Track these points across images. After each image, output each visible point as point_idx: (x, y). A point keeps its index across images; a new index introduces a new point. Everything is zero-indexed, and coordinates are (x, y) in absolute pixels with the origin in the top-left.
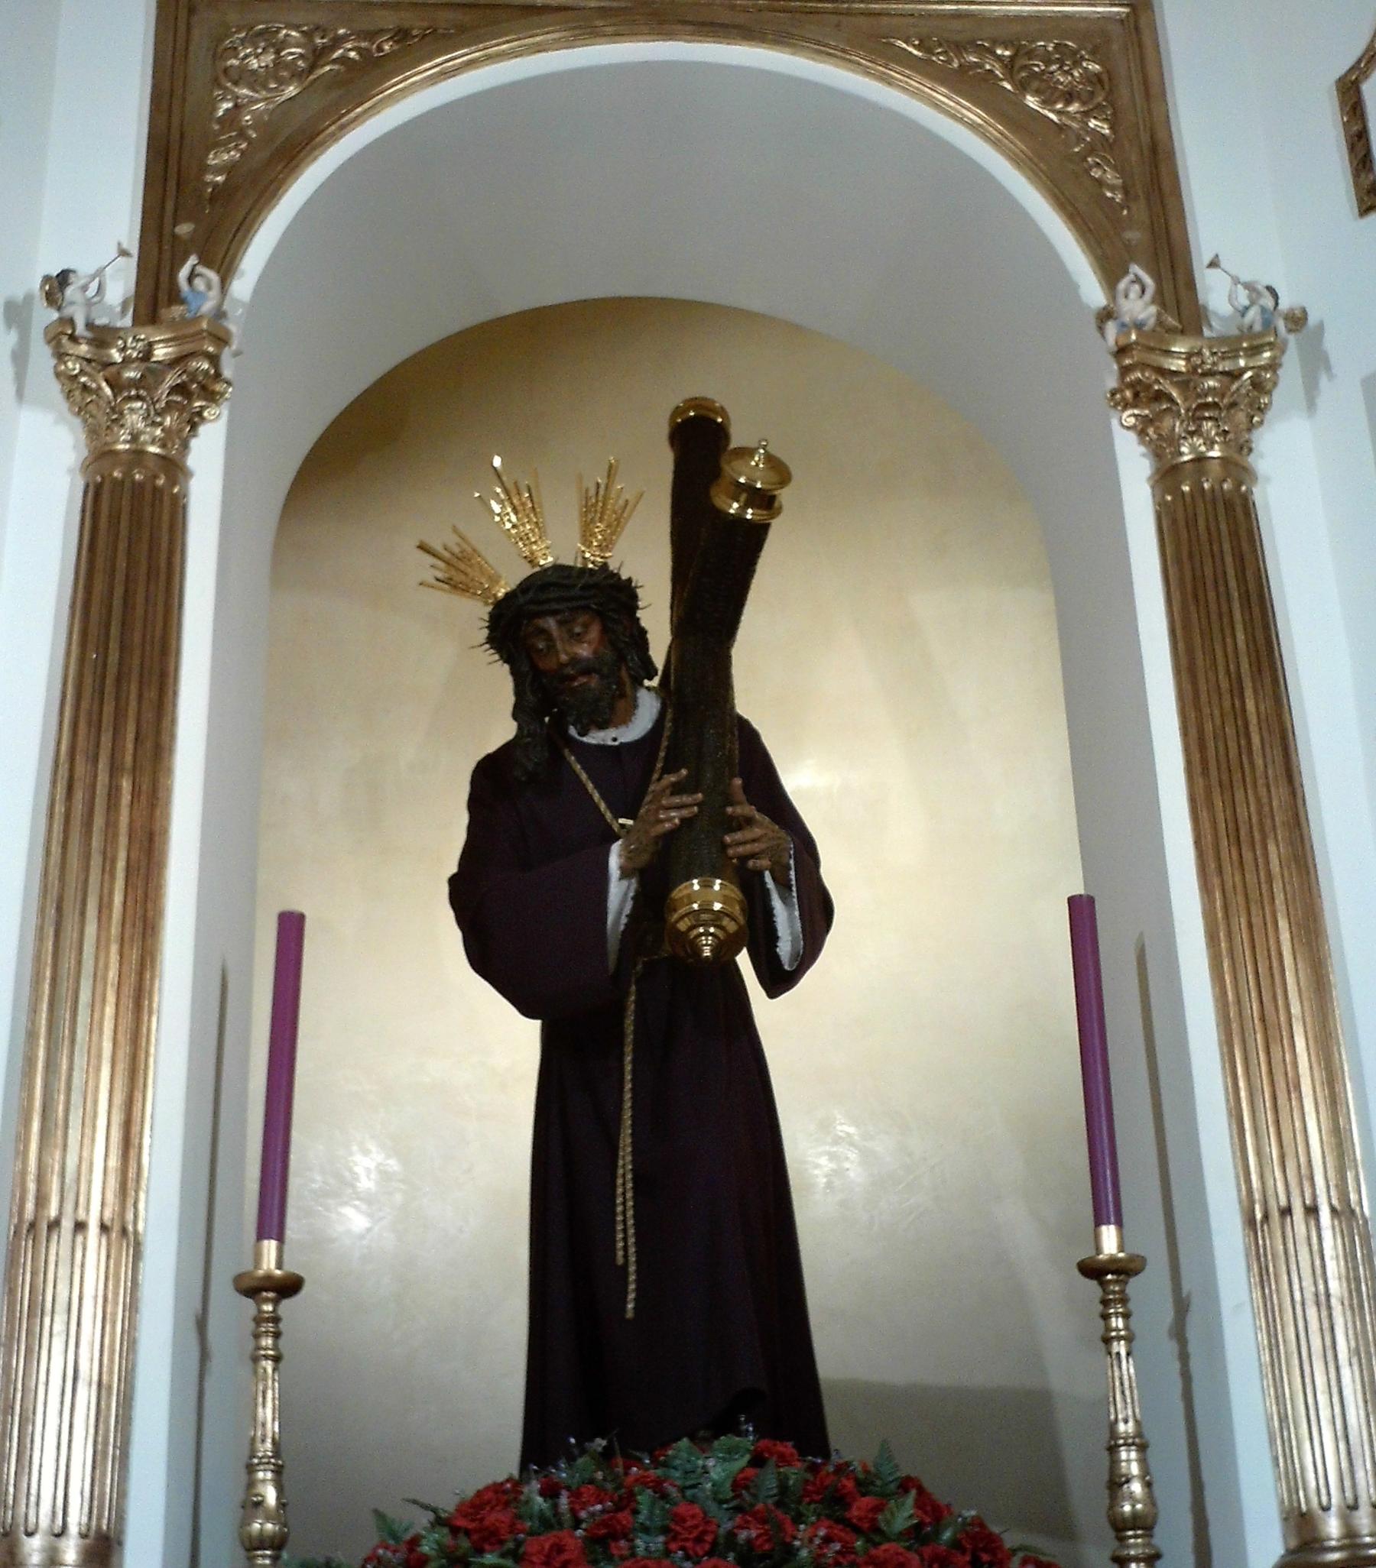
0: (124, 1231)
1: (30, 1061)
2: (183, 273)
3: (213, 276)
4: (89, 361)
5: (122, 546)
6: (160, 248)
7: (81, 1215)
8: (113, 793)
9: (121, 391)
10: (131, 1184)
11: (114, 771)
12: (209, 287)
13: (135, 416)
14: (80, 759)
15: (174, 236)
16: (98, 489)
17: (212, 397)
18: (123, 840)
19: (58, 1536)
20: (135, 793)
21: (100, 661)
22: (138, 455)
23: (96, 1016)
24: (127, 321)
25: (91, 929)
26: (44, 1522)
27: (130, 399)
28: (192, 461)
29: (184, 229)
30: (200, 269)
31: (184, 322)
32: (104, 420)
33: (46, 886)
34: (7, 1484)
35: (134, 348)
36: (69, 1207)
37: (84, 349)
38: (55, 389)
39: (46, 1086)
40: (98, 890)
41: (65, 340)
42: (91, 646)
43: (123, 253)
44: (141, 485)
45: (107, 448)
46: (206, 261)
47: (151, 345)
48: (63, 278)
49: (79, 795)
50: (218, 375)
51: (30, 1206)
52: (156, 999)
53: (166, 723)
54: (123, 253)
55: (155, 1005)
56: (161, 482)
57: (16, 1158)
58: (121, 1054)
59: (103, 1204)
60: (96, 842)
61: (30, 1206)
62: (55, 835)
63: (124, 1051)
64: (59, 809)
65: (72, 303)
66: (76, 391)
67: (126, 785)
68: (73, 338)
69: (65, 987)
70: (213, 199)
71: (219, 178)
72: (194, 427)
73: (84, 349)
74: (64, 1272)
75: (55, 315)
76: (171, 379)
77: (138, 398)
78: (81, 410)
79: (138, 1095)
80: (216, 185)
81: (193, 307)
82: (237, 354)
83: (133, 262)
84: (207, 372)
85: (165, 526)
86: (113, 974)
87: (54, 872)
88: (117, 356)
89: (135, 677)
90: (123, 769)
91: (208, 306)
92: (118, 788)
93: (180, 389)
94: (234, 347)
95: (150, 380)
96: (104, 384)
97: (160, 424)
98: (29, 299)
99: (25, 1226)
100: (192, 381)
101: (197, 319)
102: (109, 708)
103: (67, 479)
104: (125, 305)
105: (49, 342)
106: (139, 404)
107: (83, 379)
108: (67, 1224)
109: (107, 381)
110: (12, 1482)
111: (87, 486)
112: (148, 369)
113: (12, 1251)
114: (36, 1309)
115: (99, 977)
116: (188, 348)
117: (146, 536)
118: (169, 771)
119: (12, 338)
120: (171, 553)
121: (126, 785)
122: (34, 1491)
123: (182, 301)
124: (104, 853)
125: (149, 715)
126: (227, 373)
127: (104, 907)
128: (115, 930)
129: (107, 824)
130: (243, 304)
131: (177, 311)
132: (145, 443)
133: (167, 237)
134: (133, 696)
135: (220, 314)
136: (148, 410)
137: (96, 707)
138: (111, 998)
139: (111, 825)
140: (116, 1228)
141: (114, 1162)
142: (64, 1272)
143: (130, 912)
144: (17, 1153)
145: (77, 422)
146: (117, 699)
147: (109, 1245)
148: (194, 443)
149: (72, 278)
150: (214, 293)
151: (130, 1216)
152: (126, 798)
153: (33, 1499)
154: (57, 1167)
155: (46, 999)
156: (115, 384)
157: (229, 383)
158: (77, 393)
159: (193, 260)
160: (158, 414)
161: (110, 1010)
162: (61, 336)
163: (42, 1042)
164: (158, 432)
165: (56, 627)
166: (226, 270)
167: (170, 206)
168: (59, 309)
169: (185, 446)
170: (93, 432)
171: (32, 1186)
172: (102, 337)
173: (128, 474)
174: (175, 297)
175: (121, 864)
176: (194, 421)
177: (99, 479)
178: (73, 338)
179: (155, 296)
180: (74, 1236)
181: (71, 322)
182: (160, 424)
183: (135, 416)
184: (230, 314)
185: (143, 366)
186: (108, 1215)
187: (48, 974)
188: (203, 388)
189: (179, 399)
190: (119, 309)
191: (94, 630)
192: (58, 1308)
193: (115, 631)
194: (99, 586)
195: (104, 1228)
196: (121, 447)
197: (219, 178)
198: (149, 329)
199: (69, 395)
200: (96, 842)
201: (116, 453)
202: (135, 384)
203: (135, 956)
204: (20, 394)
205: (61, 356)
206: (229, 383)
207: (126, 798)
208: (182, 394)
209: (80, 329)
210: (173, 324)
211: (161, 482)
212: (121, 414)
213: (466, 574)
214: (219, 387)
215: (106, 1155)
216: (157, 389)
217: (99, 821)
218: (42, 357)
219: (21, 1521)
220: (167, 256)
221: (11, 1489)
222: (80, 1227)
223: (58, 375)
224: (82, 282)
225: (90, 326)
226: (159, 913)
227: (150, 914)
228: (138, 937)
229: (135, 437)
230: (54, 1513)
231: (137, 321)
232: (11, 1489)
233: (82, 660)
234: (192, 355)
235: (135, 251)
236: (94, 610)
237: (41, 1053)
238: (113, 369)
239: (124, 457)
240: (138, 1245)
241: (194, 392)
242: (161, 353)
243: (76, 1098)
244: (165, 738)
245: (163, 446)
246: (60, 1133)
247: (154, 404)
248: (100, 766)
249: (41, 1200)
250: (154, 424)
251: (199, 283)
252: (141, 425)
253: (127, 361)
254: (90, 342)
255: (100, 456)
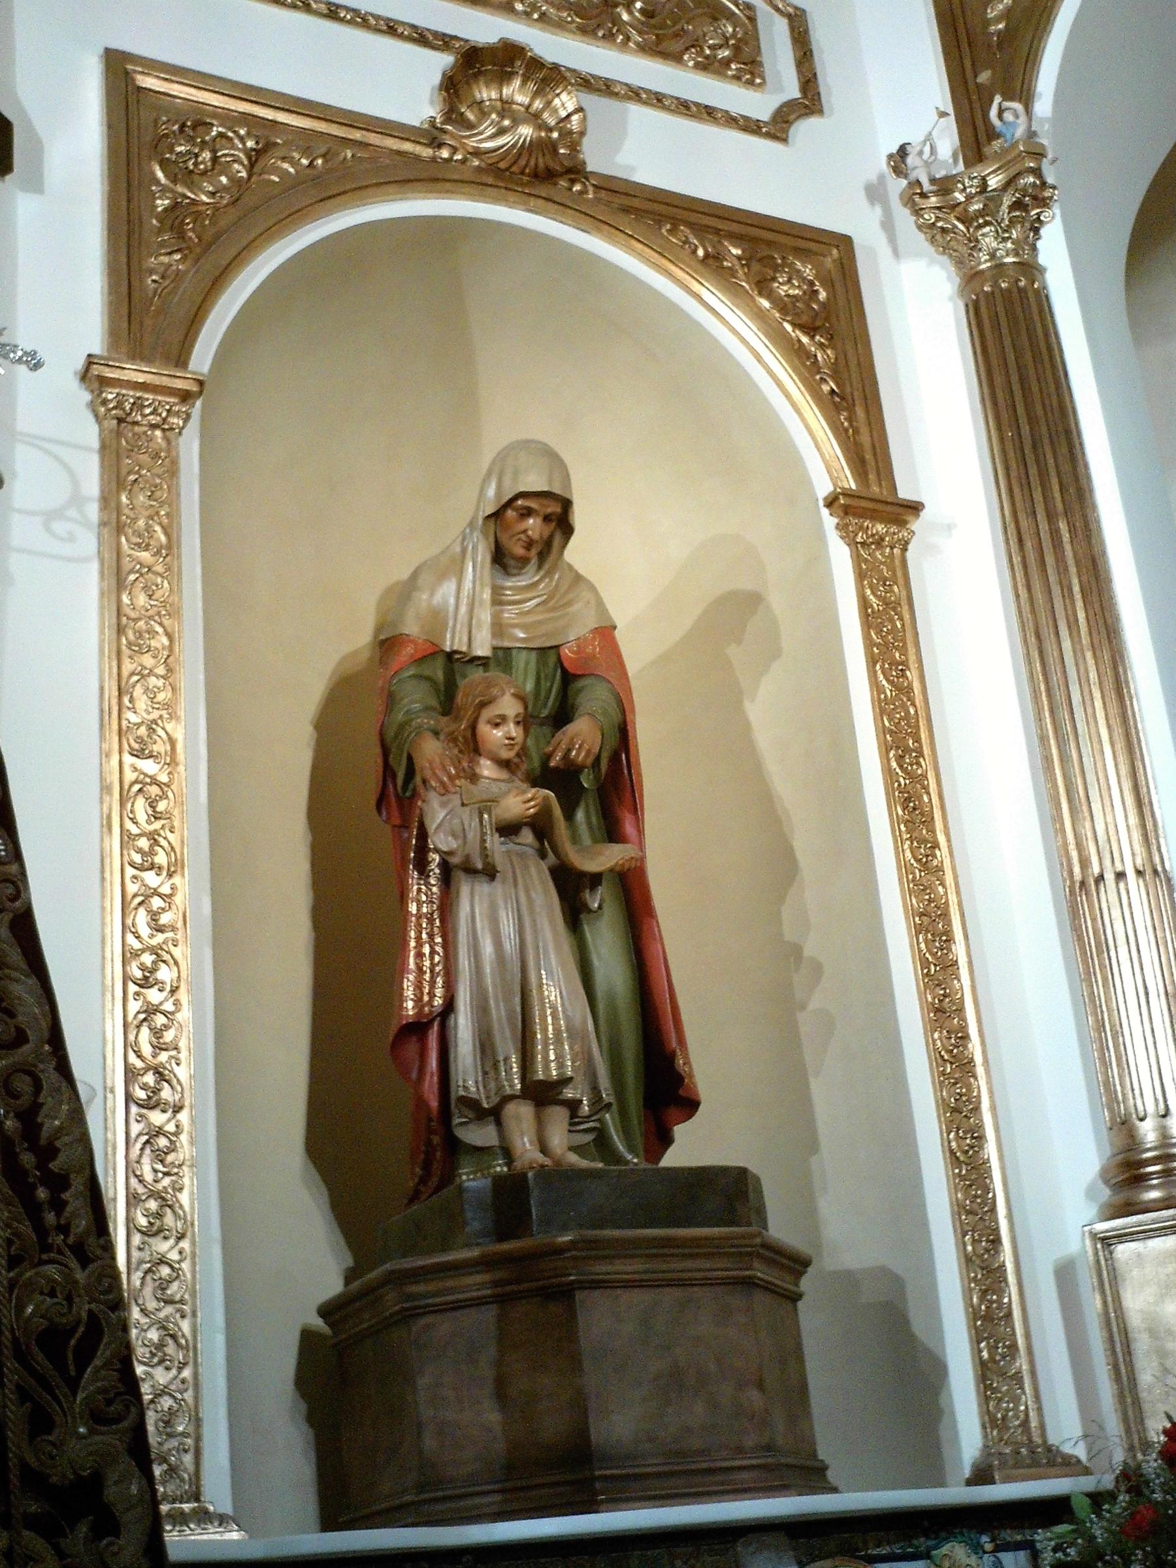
0: (1155, 872)
1: (1048, 759)
2: (993, 113)
3: (1017, 106)
4: (939, 208)
5: (1007, 342)
6: (969, 99)
7: (1119, 868)
8: (1055, 534)
9: (971, 225)
10: (1151, 835)
11: (1051, 517)
12: (1017, 117)
13: (988, 239)
14: (1022, 517)
15: (977, 85)
16: (976, 305)
17: (1044, 203)
18: (1073, 570)
19: (1164, 1116)
20: (1072, 530)
21: (1016, 437)
22: (1000, 267)
23: (1089, 711)
24: (961, 167)
25: (1067, 644)
26: (1151, 1109)
27: (980, 227)
28: (1042, 259)
29: (984, 77)
30: (1007, 104)
31: (1005, 151)
32: (964, 250)
33: (1022, 622)
34: (1115, 1086)
35: (971, 186)
36: (1107, 862)
37: (933, 200)
38: (921, 238)
39: (1065, 776)
40: (1063, 613)
41: (917, 199)
42: (1005, 427)
43: (943, 114)
44: (1009, 290)
45: (973, 272)
46: (1008, 97)
47: (984, 179)
48: (903, 151)
49: (1028, 545)
50: (1044, 183)
51: (1077, 870)
52: (1132, 687)
53: (1081, 469)
54: (943, 114)
55: (1132, 691)
56: (1022, 284)
57: (1056, 836)
58: (1116, 737)
59: (1133, 854)
60: (1053, 578)
61: (1077, 870)
62: (1018, 579)
63: (1118, 731)
64: (1017, 560)
65: (915, 168)
66: (937, 234)
67: (1063, 526)
68: (923, 195)
69: (1060, 696)
70: (1000, 45)
71: (1000, 26)
72: (1036, 231)
73: (933, 200)
74: (1116, 913)
75: (904, 182)
76: (1007, 201)
77: (987, 223)
78: (945, 249)
79: (1139, 764)
80: (999, 32)
81: (1008, 136)
82: (1054, 161)
83: (952, 117)
84: (1034, 185)
85: (1036, 318)
86: (1093, 675)
87: (1026, 608)
88: (960, 197)
89: (1046, 441)
90: (1057, 515)
91: (1020, 132)
92: (1058, 530)
93: (1018, 205)
94: (1050, 156)
95: (991, 205)
96: (956, 223)
97: (1010, 238)
98: (881, 177)
99: (1078, 885)
100: (1024, 196)
101: (1015, 145)
102: (1033, 471)
103: (950, 305)
104: (955, 156)
105: (905, 205)
106: (987, 229)
107: (940, 224)
108: (1110, 877)
109: (958, 219)
110: (1117, 1082)
111: (967, 306)
112: (988, 199)
113: (1072, 907)
114: (1103, 947)
115: (1083, 680)
116: (1013, 171)
117: (1023, 325)
118: (1094, 507)
119: (878, 210)
120: (1046, 335)
121: (1063, 526)
122: (1136, 1086)
123: (998, 136)
124: (1061, 584)
125: (1066, 467)
126: (1050, 180)
127: (1073, 625)
128: (1085, 640)
129: (1057, 561)
130: (1047, 120)
131: (996, 145)
132: (1002, 257)
133: (971, 86)
134: (1049, 456)
135: (1031, 134)
136: (997, 231)
137: (1022, 471)
138: (1097, 694)
139: (1060, 559)
140: (1149, 872)
141: (1133, 820)
142: (1116, 913)
143: (1093, 623)
144: (1056, 831)
145: (945, 259)
146: (1037, 462)
147: (1146, 886)
148: (1039, 244)
149: (908, 148)
150: (1023, 119)
151: (1157, 860)
152: (1066, 537)
153: (1137, 1092)
154: (1090, 835)
155: (1046, 708)
156: (966, 220)
157: (1054, 188)
158: (938, 237)
159: (998, 99)
160: (1005, 231)
161: (1098, 704)
162: (914, 197)
163: (1052, 742)
164: (1009, 245)
165: (975, 421)
166: (1026, 97)
167: (968, 63)
168: (906, 176)
169: (1034, 248)
170: (959, 263)
171: (1074, 854)
172: (944, 186)
173: (995, 284)
174: (993, 134)
175: (1076, 589)
176: (1036, 228)
177: (974, 297)
178: (923, 195)
179: (976, 138)
180: (1117, 884)
181: (918, 183)
182: (1010, 238)
183: (988, 239)
184: (1039, 133)
185: (982, 197)
186: (1139, 862)
187: (1043, 688)
188: (1035, 198)
189: (1018, 213)
190: (951, 161)
191: (1005, 416)
192: (1118, 943)
193: (1021, 410)
194: (999, 380)
195: (1139, 873)
196: (983, 266)
197: (1000, 26)
198: (979, 167)
199: (932, 240)
200: (1053, 578)
201: (982, 272)
202: (980, 213)
203: (1107, 657)
204: (896, 252)
205: (917, 212)
206: (1054, 188)
207: (1066, 537)
208: (1018, 209)
209: (927, 186)
210: (997, 156)
211: (1022, 284)
212: (977, 241)
213: (66, 1266)
214: (1047, 194)
215: (1126, 816)
216: (998, 212)
217: (1050, 560)
218: (904, 218)
219: (1133, 1111)
220: (977, 106)
221: (1119, 1088)
222: (1120, 876)
223: (920, 227)
224: (918, 148)
225: (933, 181)
226: (1116, 619)
227: (1109, 621)
228: (1105, 642)
229: (992, 255)
230: (1156, 1100)
231: (968, 164)
232: (1119, 1088)
233: (1002, 439)
234: (1018, 175)
235: (950, 109)
236: (1000, 396)
237: (1054, 751)
238: (960, 209)
239: (988, 274)
240: (1169, 880)
241: (1030, 204)
242: (994, 182)
243: (1091, 777)
244: (1084, 482)
245: (1017, 254)
246: (1085, 808)
247: (999, 224)
248: (1039, 517)
249: (1085, 863)
250: (1005, 240)
251: (1008, 116)
252: (994, 245)
253: (969, 198)
254: (936, 194)
255: (971, 279)
